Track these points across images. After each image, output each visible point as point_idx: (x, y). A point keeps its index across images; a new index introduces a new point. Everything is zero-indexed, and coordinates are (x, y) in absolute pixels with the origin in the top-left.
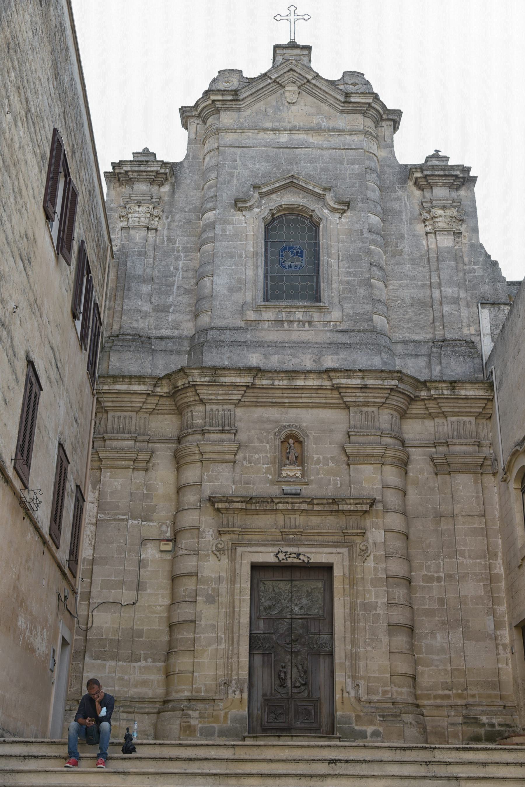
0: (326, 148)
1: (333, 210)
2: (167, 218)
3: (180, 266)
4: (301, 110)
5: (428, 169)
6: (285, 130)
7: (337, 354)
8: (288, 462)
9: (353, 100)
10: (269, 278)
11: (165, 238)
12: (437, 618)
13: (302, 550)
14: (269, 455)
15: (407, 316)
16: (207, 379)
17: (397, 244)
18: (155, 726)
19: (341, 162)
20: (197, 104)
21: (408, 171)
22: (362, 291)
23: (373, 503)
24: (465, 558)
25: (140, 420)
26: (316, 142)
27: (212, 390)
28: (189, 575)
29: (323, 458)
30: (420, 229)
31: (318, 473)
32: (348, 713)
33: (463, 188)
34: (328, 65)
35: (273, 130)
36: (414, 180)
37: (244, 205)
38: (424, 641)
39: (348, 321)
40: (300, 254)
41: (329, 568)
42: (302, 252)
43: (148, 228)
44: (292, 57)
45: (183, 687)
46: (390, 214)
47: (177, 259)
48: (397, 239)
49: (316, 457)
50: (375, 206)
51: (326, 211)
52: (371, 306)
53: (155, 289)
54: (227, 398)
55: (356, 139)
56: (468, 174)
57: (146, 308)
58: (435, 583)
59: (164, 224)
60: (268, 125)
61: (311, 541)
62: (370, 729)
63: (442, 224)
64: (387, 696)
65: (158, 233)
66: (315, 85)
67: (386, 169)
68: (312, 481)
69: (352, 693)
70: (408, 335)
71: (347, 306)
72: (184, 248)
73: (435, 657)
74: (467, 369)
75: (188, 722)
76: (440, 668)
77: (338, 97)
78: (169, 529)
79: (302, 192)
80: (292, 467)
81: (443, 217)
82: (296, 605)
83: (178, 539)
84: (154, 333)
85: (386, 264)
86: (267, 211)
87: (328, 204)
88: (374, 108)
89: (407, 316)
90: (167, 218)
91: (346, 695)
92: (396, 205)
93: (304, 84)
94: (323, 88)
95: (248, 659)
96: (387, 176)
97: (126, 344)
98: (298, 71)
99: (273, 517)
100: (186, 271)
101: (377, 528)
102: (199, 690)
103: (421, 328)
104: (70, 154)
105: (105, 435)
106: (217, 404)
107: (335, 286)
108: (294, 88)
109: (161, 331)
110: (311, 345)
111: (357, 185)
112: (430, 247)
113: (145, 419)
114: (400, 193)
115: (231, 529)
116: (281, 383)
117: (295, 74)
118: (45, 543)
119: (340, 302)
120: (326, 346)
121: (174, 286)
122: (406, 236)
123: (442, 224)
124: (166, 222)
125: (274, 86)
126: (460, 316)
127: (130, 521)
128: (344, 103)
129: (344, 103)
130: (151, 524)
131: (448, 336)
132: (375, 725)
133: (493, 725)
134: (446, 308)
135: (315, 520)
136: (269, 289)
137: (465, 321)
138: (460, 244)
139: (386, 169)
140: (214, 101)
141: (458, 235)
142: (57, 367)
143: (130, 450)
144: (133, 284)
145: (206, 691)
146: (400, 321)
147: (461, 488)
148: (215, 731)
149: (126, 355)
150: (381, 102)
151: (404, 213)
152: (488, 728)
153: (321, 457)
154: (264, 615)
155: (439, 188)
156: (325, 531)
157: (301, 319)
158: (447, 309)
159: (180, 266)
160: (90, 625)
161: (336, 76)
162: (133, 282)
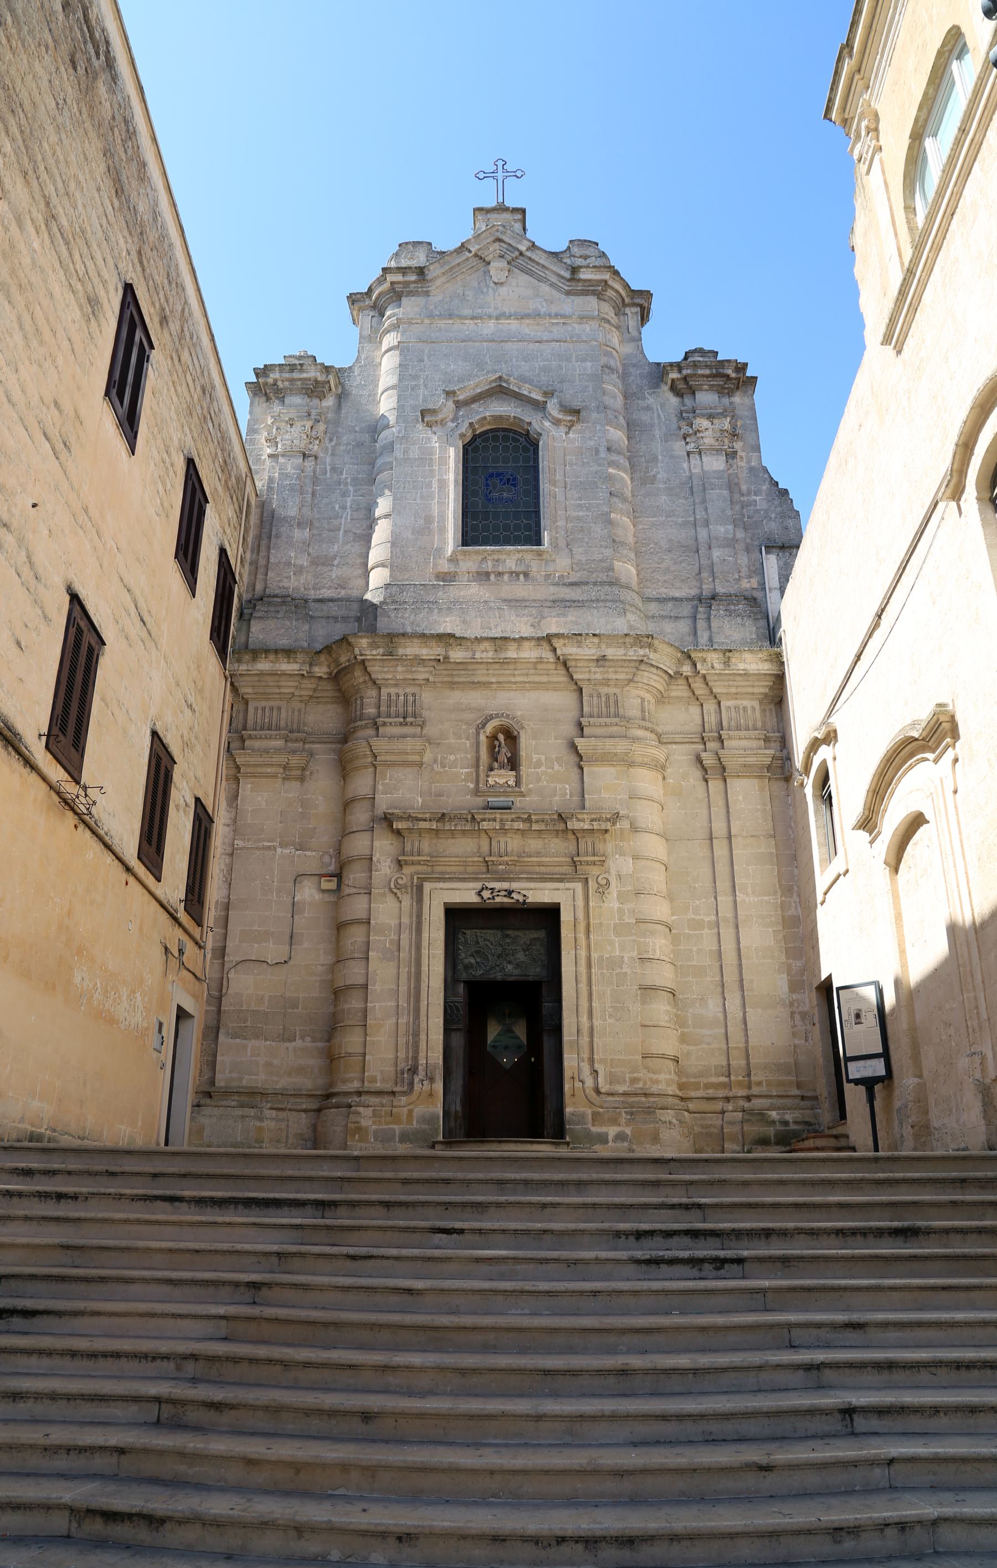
0: (547, 341)
1: (557, 422)
2: (331, 440)
3: (349, 504)
4: (516, 291)
5: (687, 367)
6: (490, 317)
7: (564, 615)
8: (496, 765)
9: (582, 276)
10: (469, 515)
11: (328, 468)
12: (709, 979)
13: (515, 885)
14: (469, 756)
15: (663, 566)
16: (381, 651)
17: (647, 468)
18: (314, 1127)
19: (568, 360)
20: (370, 290)
21: (660, 371)
22: (599, 530)
23: (616, 817)
24: (747, 894)
25: (293, 712)
26: (532, 334)
27: (868, 1073)
28: (358, 922)
29: (546, 759)
30: (679, 447)
31: (539, 780)
32: (582, 1109)
33: (738, 393)
34: (548, 232)
35: (473, 318)
36: (669, 382)
37: (433, 419)
38: (691, 1010)
39: (580, 570)
40: (512, 482)
41: (551, 914)
42: (514, 479)
43: (304, 455)
44: (503, 226)
45: (352, 1075)
46: (638, 428)
47: (344, 494)
48: (647, 462)
49: (535, 757)
50: (616, 417)
51: (547, 424)
52: (611, 550)
53: (313, 535)
54: (410, 677)
55: (588, 329)
56: (744, 374)
57: (304, 561)
58: (706, 930)
59: (327, 449)
60: (467, 312)
61: (529, 873)
62: (612, 1131)
63: (708, 440)
64: (637, 1086)
65: (318, 461)
66: (530, 259)
67: (631, 370)
68: (530, 790)
69: (589, 1082)
70: (665, 590)
71: (578, 551)
72: (353, 480)
73: (705, 1032)
74: (748, 634)
75: (358, 1122)
76: (712, 1046)
77: (562, 273)
78: (333, 860)
79: (513, 400)
80: (502, 772)
81: (710, 430)
82: (510, 962)
83: (345, 874)
84: (313, 594)
85: (633, 496)
86: (466, 424)
87: (550, 414)
88: (613, 288)
89: (663, 566)
90: (331, 440)
91: (578, 1085)
92: (645, 417)
93: (516, 258)
94: (542, 262)
95: (441, 1037)
96: (632, 378)
97: (272, 609)
98: (507, 240)
99: (476, 840)
100: (357, 511)
101: (622, 854)
102: (373, 1080)
103: (682, 581)
104: (156, 319)
105: (243, 732)
106: (396, 685)
107: (561, 523)
108: (503, 264)
109: (322, 592)
110: (528, 604)
111: (591, 389)
112: (693, 471)
113: (299, 710)
114: (651, 400)
115: (416, 858)
116: (484, 655)
117: (502, 244)
118: (128, 869)
119: (568, 545)
120: (549, 604)
121: (339, 530)
122: (660, 457)
123: (708, 440)
124: (329, 446)
125: (475, 261)
126: (736, 563)
127: (279, 850)
128: (569, 280)
129: (569, 280)
130: (308, 853)
131: (720, 590)
132: (619, 1125)
133: (786, 1123)
134: (716, 554)
135: (534, 844)
136: (469, 529)
137: (744, 571)
138: (735, 467)
139: (631, 370)
140: (392, 283)
141: (731, 455)
142: (142, 620)
143: (278, 751)
144: (282, 529)
145: (383, 1080)
146: (653, 572)
147: (740, 798)
148: (395, 1134)
149: (271, 624)
150: (622, 279)
151: (657, 428)
152: (779, 1127)
153: (543, 757)
154: (464, 976)
155: (704, 393)
156: (547, 859)
157: (514, 569)
158: (718, 554)
159: (349, 504)
160: (224, 991)
161: (560, 246)
162: (283, 526)
